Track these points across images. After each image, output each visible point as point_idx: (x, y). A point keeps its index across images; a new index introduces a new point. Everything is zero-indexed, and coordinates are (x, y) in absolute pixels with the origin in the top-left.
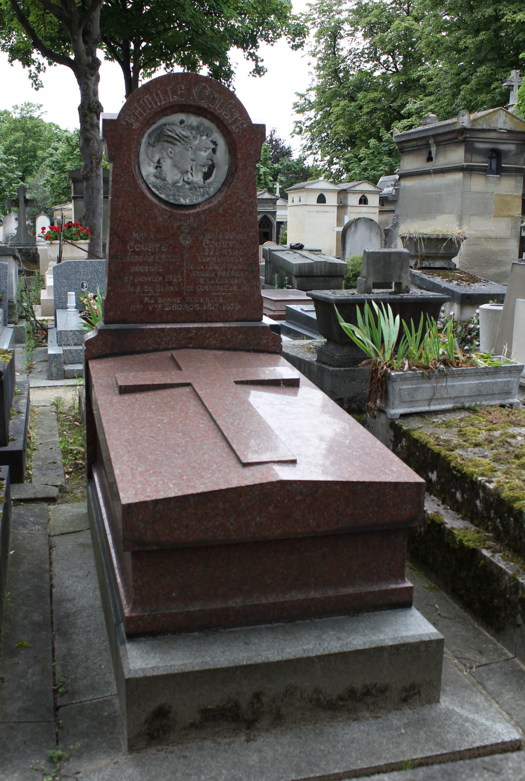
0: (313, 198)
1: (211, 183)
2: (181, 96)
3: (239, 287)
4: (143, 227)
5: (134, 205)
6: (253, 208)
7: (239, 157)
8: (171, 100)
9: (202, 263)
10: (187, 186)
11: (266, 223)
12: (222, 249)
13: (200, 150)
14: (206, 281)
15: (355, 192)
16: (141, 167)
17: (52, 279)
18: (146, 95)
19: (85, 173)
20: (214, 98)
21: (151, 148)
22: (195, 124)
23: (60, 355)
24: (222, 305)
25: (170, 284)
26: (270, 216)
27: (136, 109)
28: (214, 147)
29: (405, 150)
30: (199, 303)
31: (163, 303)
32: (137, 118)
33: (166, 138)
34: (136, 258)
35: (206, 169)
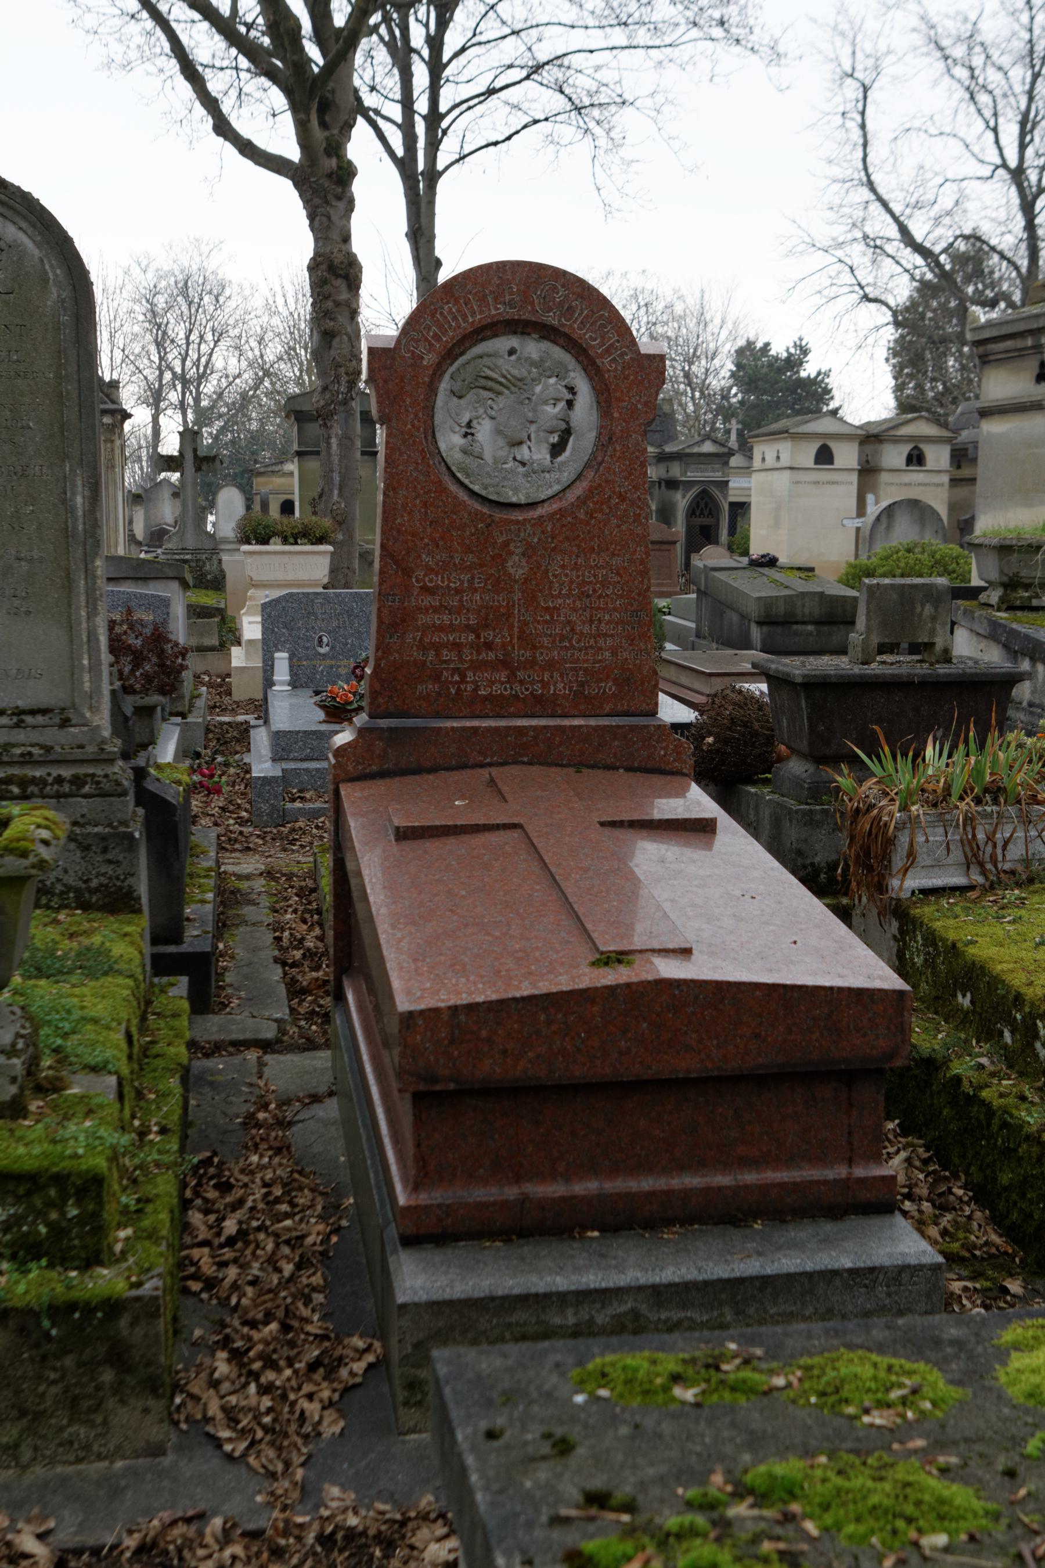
0: (807, 455)
1: (563, 463)
2: (511, 304)
3: (614, 652)
4: (441, 543)
5: (425, 504)
6: (641, 509)
7: (616, 415)
8: (493, 312)
9: (547, 609)
10: (521, 469)
11: (706, 505)
12: (585, 583)
13: (545, 402)
14: (554, 641)
15: (898, 440)
16: (438, 434)
17: (259, 627)
18: (448, 303)
19: (322, 403)
20: (570, 308)
21: (455, 399)
22: (535, 356)
23: (274, 779)
24: (582, 684)
25: (489, 646)
26: (715, 492)
27: (429, 329)
28: (570, 397)
29: (992, 358)
30: (542, 681)
31: (475, 682)
32: (431, 345)
33: (483, 382)
34: (427, 600)
35: (555, 439)
